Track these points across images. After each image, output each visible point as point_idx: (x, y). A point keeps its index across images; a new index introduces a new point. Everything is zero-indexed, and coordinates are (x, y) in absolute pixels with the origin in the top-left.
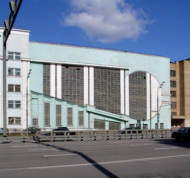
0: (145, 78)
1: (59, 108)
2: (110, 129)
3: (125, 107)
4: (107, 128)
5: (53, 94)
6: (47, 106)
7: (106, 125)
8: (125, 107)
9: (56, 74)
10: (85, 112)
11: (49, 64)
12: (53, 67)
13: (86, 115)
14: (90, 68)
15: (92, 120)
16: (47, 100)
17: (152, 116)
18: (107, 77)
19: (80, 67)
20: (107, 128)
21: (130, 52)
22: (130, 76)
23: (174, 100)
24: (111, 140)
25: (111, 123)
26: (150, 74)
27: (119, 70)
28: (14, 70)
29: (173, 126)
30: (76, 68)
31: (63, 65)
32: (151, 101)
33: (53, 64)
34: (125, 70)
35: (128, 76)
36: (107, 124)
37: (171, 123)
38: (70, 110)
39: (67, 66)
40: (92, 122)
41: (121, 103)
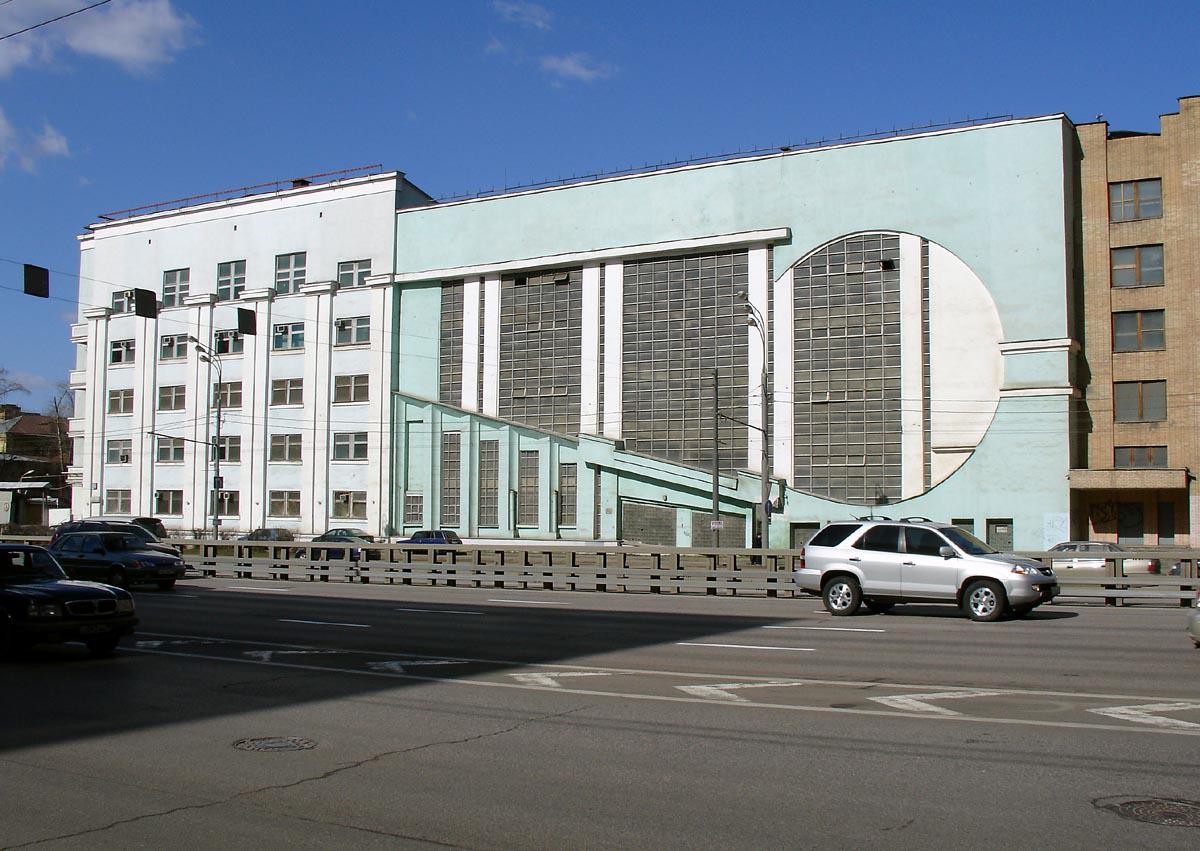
0: (890, 265)
1: (489, 449)
2: (695, 543)
3: (775, 441)
4: (684, 540)
5: (469, 402)
6: (450, 443)
7: (679, 524)
8: (775, 441)
9: (484, 312)
10: (582, 469)
11: (459, 282)
12: (471, 290)
13: (585, 477)
14: (607, 267)
15: (609, 502)
16: (450, 423)
17: (935, 478)
18: (685, 292)
19: (566, 274)
20: (684, 540)
21: (808, 145)
22: (799, 269)
23: (1139, 365)
24: (464, 586)
25: (700, 518)
26: (925, 241)
27: (742, 249)
28: (354, 323)
29: (1173, 537)
30: (549, 280)
31: (505, 276)
32: (926, 392)
33: (471, 278)
34: (770, 245)
35: (789, 276)
36: (684, 519)
37: (1068, 515)
38: (529, 459)
39: (518, 277)
40: (609, 511)
41: (790, 397)
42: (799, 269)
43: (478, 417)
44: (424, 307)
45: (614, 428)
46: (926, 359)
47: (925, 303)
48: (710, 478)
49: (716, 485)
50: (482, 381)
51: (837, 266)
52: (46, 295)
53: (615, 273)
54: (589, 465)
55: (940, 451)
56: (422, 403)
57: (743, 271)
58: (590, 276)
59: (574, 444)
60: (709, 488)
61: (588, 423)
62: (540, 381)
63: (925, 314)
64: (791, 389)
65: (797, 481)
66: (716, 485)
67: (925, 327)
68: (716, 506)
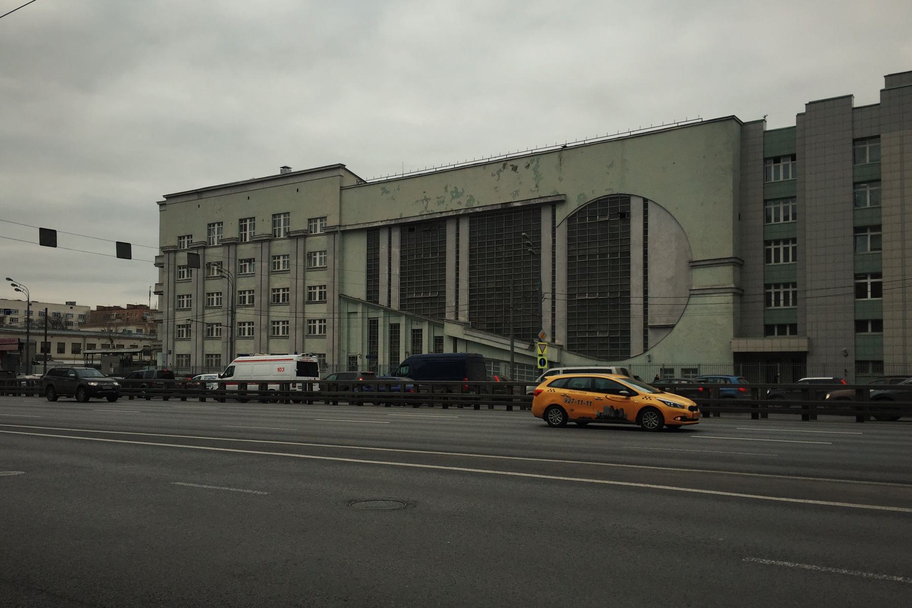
1: (394, 330)
5: (383, 300)
6: (373, 325)
9: (391, 251)
35: (565, 224)
42: (570, 219)
43: (388, 311)
44: (357, 249)
45: (463, 317)
46: (646, 272)
47: (645, 238)
48: (509, 342)
49: (512, 347)
50: (390, 290)
51: (592, 217)
52: (130, 258)
53: (465, 227)
54: (450, 337)
55: (653, 327)
56: (356, 301)
57: (538, 220)
58: (450, 229)
59: (442, 326)
60: (509, 348)
61: (449, 315)
62: (422, 293)
63: (645, 245)
64: (565, 292)
65: (568, 345)
66: (512, 347)
67: (645, 252)
68: (512, 359)
